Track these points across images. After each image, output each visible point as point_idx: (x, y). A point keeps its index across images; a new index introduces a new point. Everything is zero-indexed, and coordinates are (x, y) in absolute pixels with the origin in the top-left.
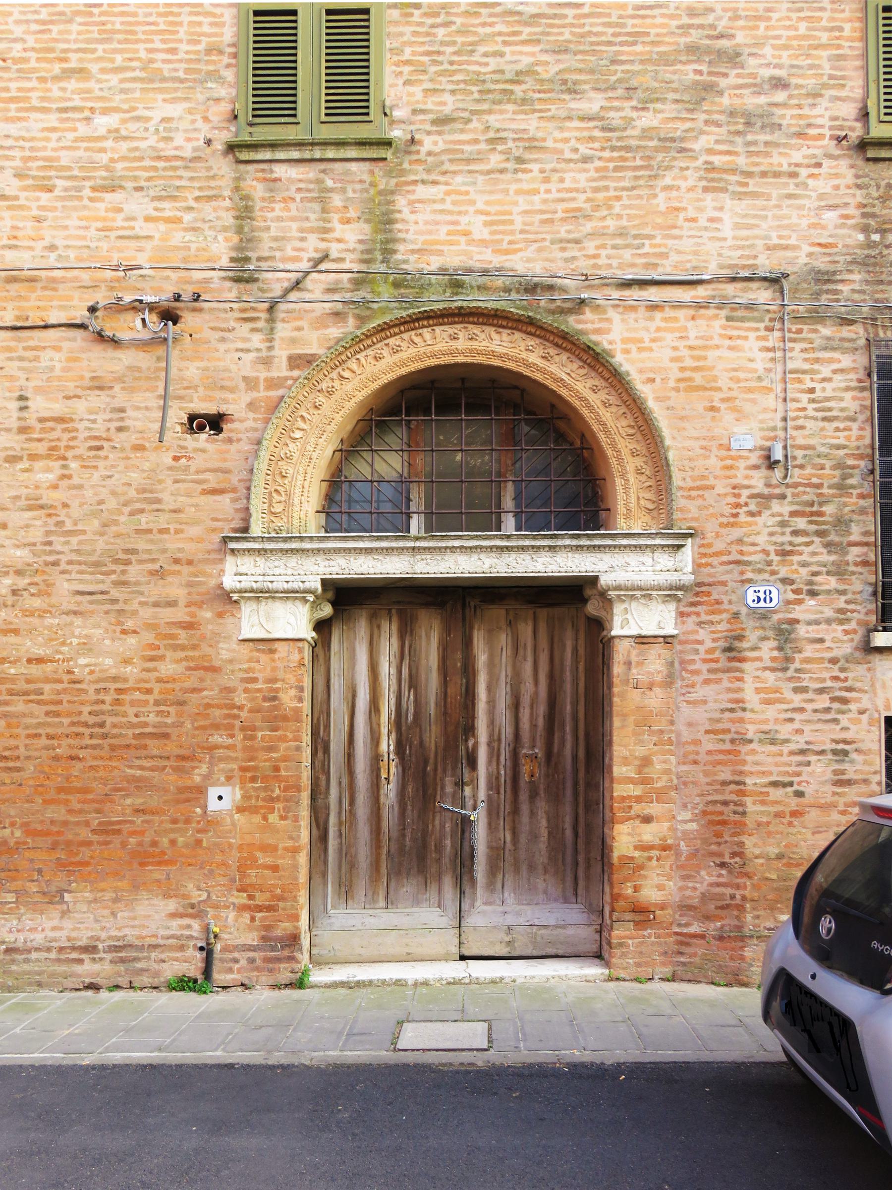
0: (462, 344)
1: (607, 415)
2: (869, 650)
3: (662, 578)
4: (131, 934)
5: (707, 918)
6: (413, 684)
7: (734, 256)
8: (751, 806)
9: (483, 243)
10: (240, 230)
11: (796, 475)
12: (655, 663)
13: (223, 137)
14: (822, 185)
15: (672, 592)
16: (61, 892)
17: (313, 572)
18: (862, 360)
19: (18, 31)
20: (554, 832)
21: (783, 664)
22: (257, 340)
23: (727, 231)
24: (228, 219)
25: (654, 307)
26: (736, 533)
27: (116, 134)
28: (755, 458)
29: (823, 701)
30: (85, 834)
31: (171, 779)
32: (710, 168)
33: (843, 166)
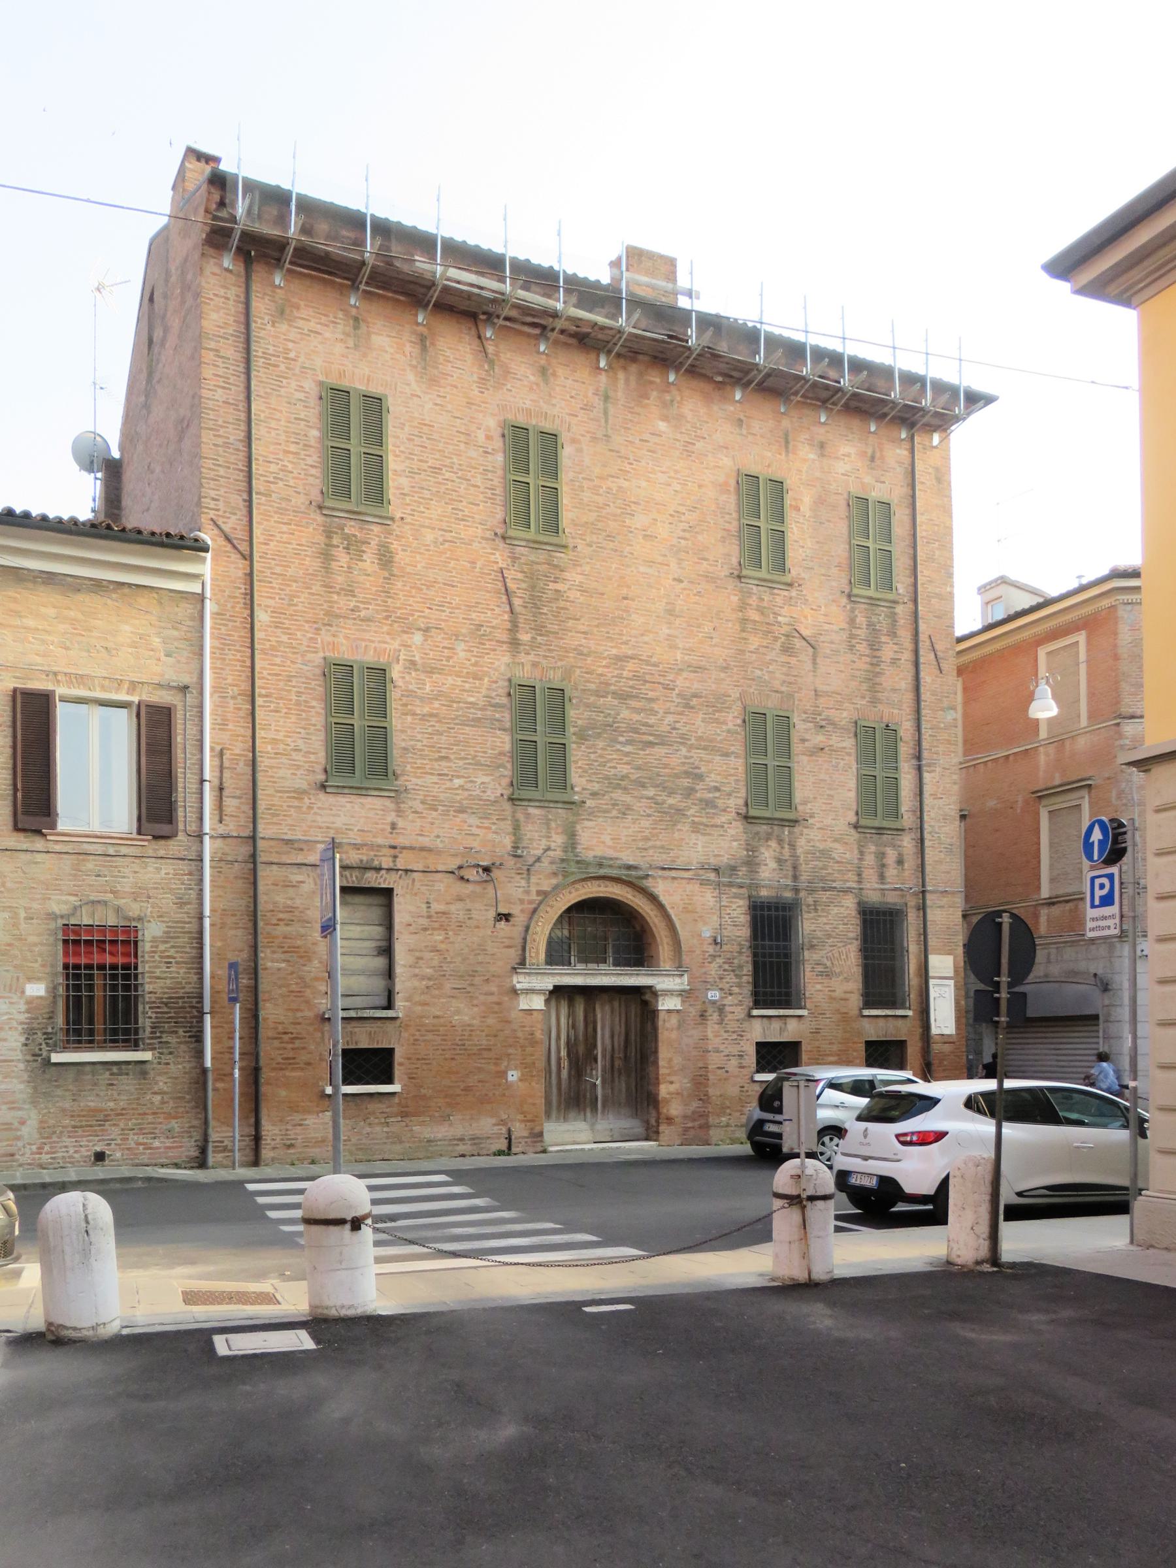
0: (602, 889)
1: (656, 920)
2: (750, 1016)
3: (677, 987)
4: (478, 1132)
5: (694, 1120)
6: (574, 1027)
7: (702, 859)
8: (711, 1077)
9: (609, 847)
10: (515, 834)
11: (725, 948)
12: (674, 1020)
13: (507, 793)
14: (732, 832)
15: (682, 994)
16: (449, 1116)
17: (549, 983)
18: (747, 903)
19: (419, 737)
20: (628, 1089)
21: (721, 1023)
22: (523, 883)
23: (700, 849)
24: (510, 829)
25: (674, 878)
26: (703, 970)
27: (461, 787)
28: (710, 941)
29: (735, 1036)
30: (458, 1091)
31: (492, 1068)
32: (694, 822)
33: (739, 824)
